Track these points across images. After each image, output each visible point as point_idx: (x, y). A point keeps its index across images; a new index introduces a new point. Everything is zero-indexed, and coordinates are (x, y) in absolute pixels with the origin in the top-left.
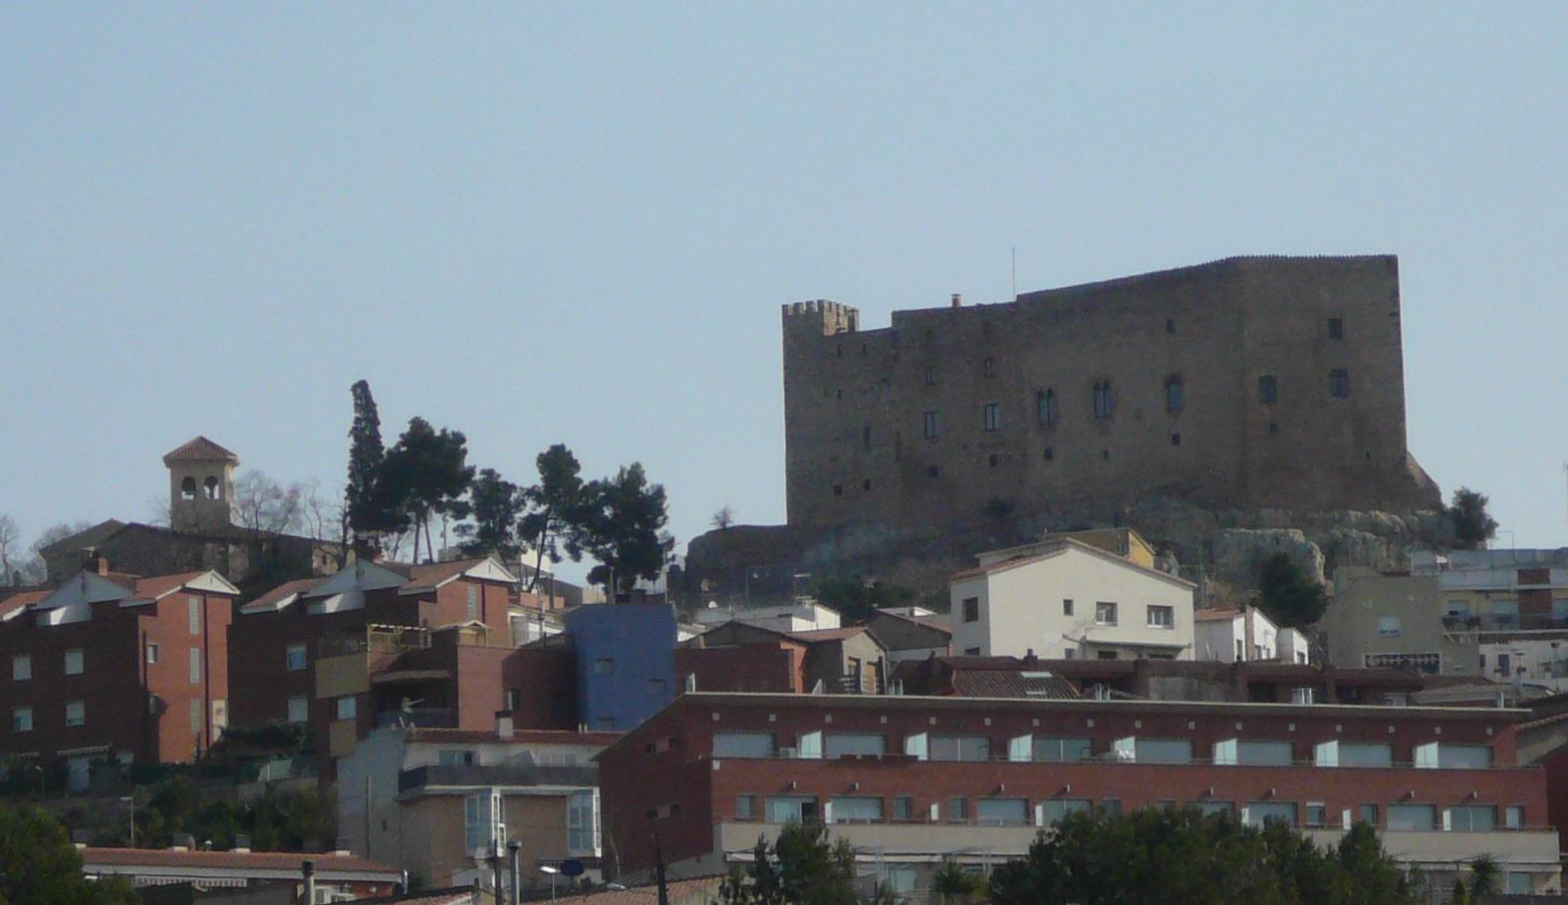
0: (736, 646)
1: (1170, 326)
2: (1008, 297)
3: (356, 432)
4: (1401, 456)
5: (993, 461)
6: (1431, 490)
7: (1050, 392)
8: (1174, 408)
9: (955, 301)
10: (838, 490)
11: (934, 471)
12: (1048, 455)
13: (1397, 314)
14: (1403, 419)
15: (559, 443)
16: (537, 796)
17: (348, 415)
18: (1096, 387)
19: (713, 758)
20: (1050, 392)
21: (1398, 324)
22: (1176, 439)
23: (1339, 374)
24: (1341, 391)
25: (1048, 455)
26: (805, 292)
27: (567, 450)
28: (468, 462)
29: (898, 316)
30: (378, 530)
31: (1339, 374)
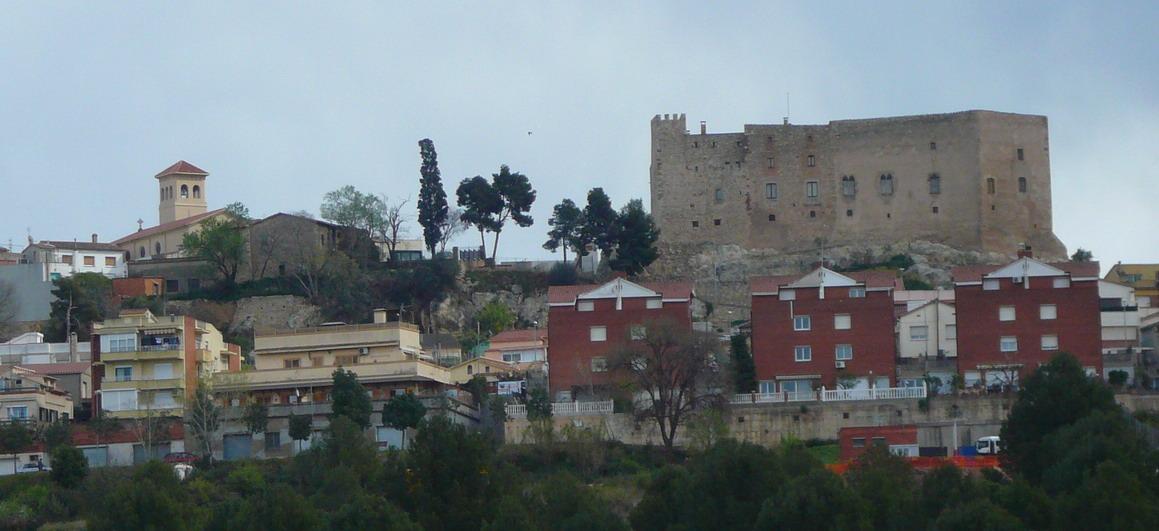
0: (778, 378)
1: (933, 146)
2: (824, 121)
3: (423, 170)
4: (1049, 230)
5: (813, 214)
6: (1063, 249)
7: (852, 179)
8: (935, 192)
9: (786, 121)
10: (695, 224)
11: (772, 218)
12: (850, 213)
13: (1047, 149)
14: (1050, 208)
15: (1087, 250)
16: (401, 382)
17: (419, 161)
18: (883, 178)
19: (668, 442)
20: (852, 179)
21: (1048, 155)
22: (935, 210)
23: (1022, 180)
24: (1023, 189)
25: (850, 213)
26: (669, 109)
27: (1094, 259)
28: (581, 210)
29: (748, 127)
30: (732, 344)
31: (1022, 180)
